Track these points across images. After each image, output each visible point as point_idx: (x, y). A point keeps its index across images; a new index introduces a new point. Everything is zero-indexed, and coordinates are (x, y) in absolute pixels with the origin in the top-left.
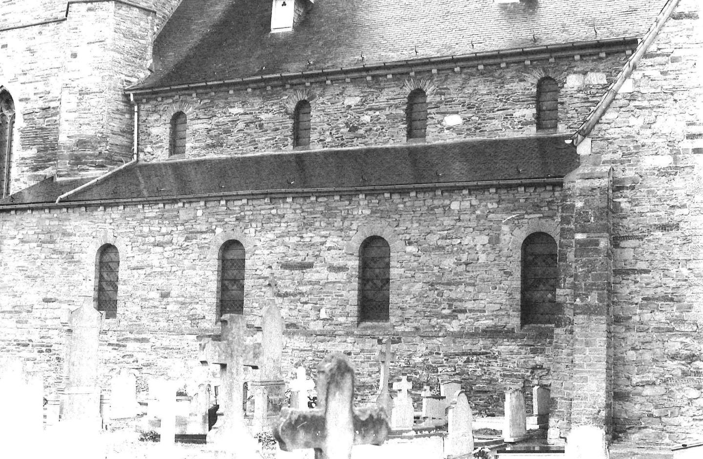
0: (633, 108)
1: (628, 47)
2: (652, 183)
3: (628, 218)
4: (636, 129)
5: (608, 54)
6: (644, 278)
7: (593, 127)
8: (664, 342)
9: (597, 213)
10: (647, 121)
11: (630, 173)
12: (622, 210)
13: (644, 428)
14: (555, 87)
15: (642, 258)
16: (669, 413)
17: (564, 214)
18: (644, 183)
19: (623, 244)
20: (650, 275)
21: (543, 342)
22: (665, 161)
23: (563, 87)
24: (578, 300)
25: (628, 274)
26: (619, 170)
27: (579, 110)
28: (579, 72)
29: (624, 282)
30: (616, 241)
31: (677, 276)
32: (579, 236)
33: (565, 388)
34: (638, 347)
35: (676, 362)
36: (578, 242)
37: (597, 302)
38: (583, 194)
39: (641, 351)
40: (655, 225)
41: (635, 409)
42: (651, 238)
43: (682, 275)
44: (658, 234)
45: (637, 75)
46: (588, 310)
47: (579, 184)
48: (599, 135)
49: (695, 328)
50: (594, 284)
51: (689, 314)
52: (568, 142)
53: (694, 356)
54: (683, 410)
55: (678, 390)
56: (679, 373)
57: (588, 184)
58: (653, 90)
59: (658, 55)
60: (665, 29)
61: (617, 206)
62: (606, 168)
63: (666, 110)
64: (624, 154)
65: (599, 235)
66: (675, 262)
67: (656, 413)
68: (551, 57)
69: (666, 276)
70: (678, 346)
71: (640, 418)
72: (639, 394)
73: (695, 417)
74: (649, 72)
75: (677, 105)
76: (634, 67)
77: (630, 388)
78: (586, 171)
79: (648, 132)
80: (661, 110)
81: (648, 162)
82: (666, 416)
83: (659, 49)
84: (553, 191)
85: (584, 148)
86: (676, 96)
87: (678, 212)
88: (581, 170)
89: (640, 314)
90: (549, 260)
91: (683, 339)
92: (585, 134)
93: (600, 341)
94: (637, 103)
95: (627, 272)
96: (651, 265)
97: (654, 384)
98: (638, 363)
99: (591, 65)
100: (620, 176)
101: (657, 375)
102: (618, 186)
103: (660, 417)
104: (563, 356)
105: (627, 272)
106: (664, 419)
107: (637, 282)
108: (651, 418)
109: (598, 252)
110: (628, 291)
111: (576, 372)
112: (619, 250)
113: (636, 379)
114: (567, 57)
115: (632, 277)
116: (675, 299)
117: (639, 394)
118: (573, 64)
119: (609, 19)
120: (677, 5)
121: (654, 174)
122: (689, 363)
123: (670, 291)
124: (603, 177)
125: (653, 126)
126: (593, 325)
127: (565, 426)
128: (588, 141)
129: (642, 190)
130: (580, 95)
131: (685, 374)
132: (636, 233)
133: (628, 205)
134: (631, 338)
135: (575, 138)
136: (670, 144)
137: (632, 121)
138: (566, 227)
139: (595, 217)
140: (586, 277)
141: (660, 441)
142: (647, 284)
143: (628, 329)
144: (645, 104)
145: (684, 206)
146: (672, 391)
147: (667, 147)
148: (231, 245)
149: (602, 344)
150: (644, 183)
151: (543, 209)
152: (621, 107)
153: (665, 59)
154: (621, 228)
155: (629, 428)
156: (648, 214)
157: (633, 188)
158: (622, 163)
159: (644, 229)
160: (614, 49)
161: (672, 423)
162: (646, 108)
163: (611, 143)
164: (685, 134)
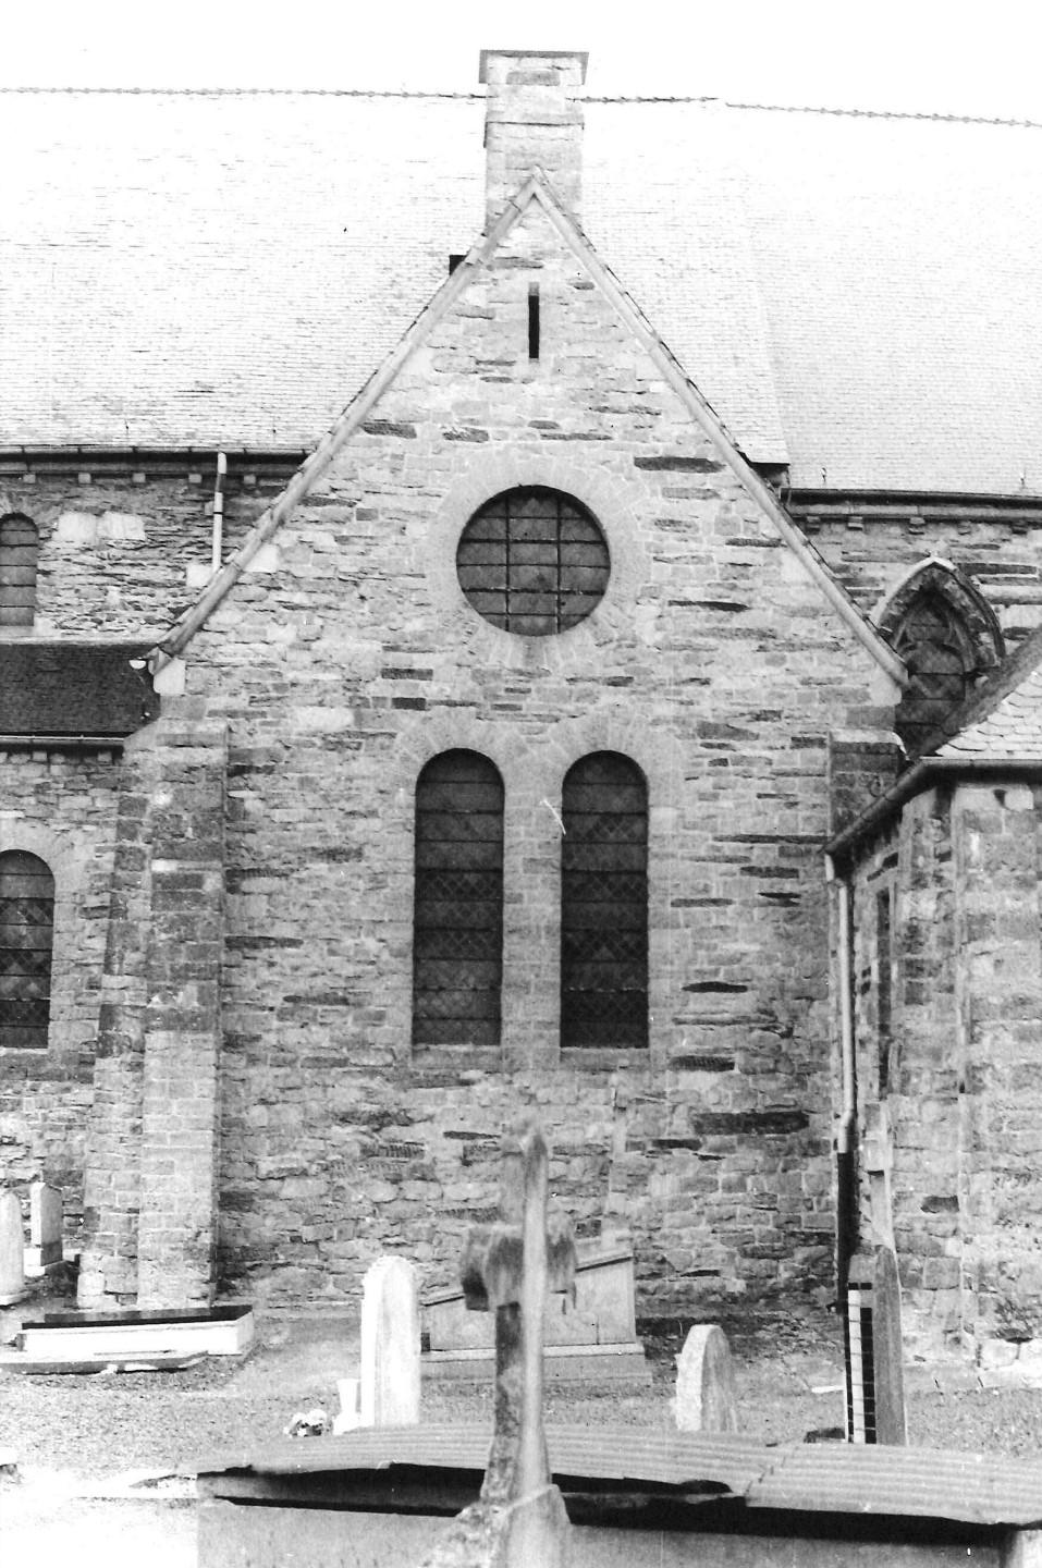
0: (275, 606)
1: (194, 468)
2: (309, 763)
3: (260, 833)
4: (280, 647)
5: (150, 477)
6: (286, 957)
7: (190, 638)
8: (325, 1086)
9: (200, 819)
10: (304, 634)
11: (264, 740)
12: (246, 814)
13: (282, 1265)
14: (29, 538)
15: (286, 916)
16: (335, 1233)
17: (124, 818)
18: (294, 762)
19: (246, 885)
20: (300, 951)
21: (18, 1086)
22: (338, 718)
23: (48, 539)
24: (156, 999)
25: (255, 947)
26: (242, 732)
27: (83, 590)
28: (88, 510)
29: (247, 962)
30: (234, 878)
31: (356, 953)
32: (162, 867)
33: (116, 1187)
34: (273, 1099)
35: (349, 1129)
36: (157, 878)
37: (196, 1004)
38: (170, 777)
39: (278, 1107)
40: (313, 849)
41: (263, 1226)
42: (304, 874)
43: (367, 953)
44: (320, 867)
45: (286, 538)
46: (177, 1022)
47: (163, 756)
48: (203, 656)
49: (389, 1058)
50: (187, 968)
51: (377, 1030)
52: (137, 664)
53: (386, 1114)
54: (362, 1225)
55: (355, 1185)
56: (356, 1150)
57: (181, 756)
58: (320, 573)
59: (333, 502)
60: (349, 452)
61: (235, 804)
62: (219, 726)
63: (343, 615)
64: (252, 700)
65: (203, 864)
66: (353, 926)
67: (308, 1233)
68: (29, 472)
69: (332, 952)
70: (356, 1095)
71: (275, 1245)
72: (273, 1196)
73: (388, 1240)
74: (310, 534)
75: (366, 607)
76: (281, 522)
77: (253, 1185)
78: (177, 731)
79: (307, 658)
80: (331, 614)
81: (307, 718)
82: (329, 1239)
83: (334, 490)
84: (48, 763)
85: (170, 681)
86: (364, 589)
87: (360, 824)
88: (162, 726)
89: (279, 1030)
90: (37, 913)
91: (364, 1081)
92: (174, 650)
93: (203, 1086)
94: (283, 596)
95: (255, 943)
96: (303, 928)
97: (304, 1173)
98: (270, 1131)
99: (114, 497)
100: (245, 743)
101: (310, 1156)
102: (239, 768)
103: (316, 1243)
104: (114, 1119)
105: (255, 943)
106: (324, 1246)
107: (272, 964)
108: (298, 1245)
109: (198, 899)
110: (254, 983)
111: (148, 1152)
112: (237, 898)
113: (267, 1165)
114: (64, 475)
115: (264, 953)
116: (351, 999)
117: (273, 1196)
118: (74, 491)
119: (153, 404)
120: (375, 404)
121: (314, 745)
122: (376, 1131)
123: (343, 984)
124: (211, 746)
125: (314, 645)
126: (188, 1053)
127: (117, 1268)
128: (178, 665)
129: (289, 775)
130: (89, 558)
131: (367, 1152)
132: (275, 864)
133: (259, 804)
134: (257, 1080)
135: (152, 658)
136: (349, 685)
137: (275, 632)
138: (128, 844)
139: (195, 828)
140: (174, 950)
141: (316, 1292)
142: (296, 969)
143: (253, 1060)
144: (299, 598)
145: (373, 814)
146: (342, 1188)
147: (341, 691)
148: (673, 904)
149: (206, 1092)
150: (294, 762)
151: (25, 801)
152: (250, 601)
153: (345, 509)
154: (244, 852)
155: (252, 1268)
156: (301, 826)
157: (269, 770)
158: (248, 716)
159: (292, 857)
160: (163, 468)
161: (341, 1253)
162: (303, 608)
163: (227, 674)
164: (381, 667)
